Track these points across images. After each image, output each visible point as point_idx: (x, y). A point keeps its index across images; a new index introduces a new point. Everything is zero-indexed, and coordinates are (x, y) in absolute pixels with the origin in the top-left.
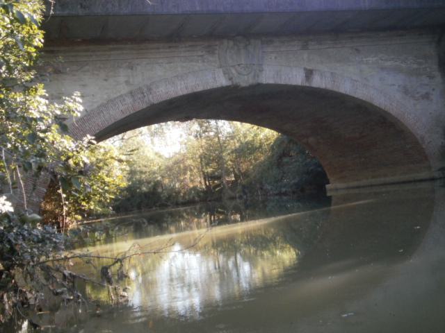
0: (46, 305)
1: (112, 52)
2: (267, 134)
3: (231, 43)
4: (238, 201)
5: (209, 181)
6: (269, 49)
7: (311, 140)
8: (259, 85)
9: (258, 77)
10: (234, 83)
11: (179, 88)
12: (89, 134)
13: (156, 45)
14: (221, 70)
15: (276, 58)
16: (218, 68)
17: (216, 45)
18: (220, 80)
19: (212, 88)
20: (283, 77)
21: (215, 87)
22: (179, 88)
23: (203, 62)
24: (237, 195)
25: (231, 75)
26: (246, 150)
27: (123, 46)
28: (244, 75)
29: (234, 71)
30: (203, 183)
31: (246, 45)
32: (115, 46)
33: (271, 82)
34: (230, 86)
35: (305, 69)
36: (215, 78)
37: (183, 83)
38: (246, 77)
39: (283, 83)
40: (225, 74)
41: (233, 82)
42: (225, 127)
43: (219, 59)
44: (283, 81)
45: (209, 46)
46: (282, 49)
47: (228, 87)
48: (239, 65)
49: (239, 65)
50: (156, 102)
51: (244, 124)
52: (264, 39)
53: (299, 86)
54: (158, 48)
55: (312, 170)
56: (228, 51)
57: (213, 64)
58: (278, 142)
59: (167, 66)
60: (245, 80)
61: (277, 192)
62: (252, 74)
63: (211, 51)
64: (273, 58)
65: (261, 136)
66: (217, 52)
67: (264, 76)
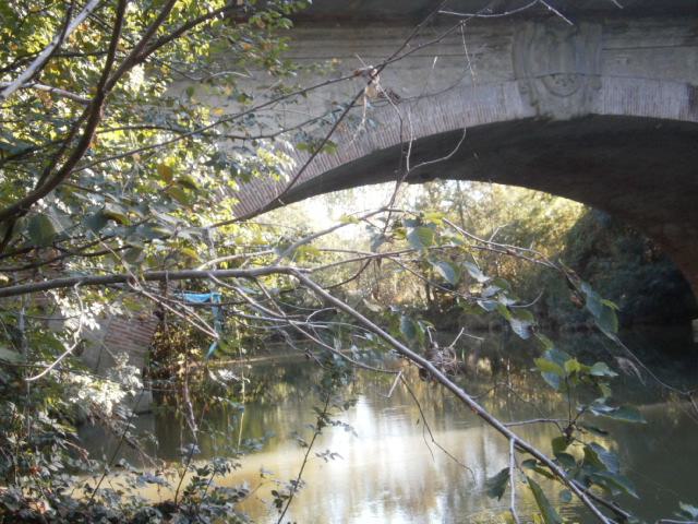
0: (70, 212)
1: (304, 44)
2: (565, 210)
3: (541, 30)
4: (492, 334)
5: (434, 292)
6: (618, 44)
7: (671, 229)
8: (591, 116)
9: (591, 99)
10: (542, 113)
11: (430, 118)
12: (490, 359)
13: (386, 31)
14: (516, 84)
15: (628, 61)
16: (510, 80)
17: (511, 34)
18: (506, 104)
19: (494, 120)
20: (642, 103)
21: (502, 119)
22: (430, 118)
23: (480, 66)
24: (491, 323)
25: (535, 97)
26: (521, 235)
27: (325, 31)
28: (563, 97)
29: (542, 89)
30: (424, 296)
31: (571, 35)
32: (309, 31)
33: (616, 111)
34: (532, 118)
35: (689, 86)
36: (502, 101)
37: (438, 109)
38: (566, 100)
39: (640, 114)
40: (522, 93)
41: (538, 109)
42: (478, 193)
43: (514, 59)
44: (642, 109)
45: (495, 35)
46: (643, 44)
47: (527, 121)
48: (553, 75)
49: (553, 75)
50: (383, 145)
51: (512, 187)
52: (607, 21)
53: (674, 121)
54: (393, 38)
55: (655, 286)
56: (533, 47)
57: (501, 73)
58: (583, 227)
59: (409, 73)
60: (563, 108)
61: (575, 325)
62: (578, 96)
63: (497, 45)
64: (624, 61)
65: (548, 213)
66: (510, 47)
67: (602, 98)
